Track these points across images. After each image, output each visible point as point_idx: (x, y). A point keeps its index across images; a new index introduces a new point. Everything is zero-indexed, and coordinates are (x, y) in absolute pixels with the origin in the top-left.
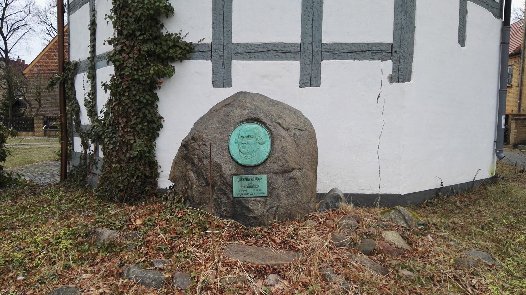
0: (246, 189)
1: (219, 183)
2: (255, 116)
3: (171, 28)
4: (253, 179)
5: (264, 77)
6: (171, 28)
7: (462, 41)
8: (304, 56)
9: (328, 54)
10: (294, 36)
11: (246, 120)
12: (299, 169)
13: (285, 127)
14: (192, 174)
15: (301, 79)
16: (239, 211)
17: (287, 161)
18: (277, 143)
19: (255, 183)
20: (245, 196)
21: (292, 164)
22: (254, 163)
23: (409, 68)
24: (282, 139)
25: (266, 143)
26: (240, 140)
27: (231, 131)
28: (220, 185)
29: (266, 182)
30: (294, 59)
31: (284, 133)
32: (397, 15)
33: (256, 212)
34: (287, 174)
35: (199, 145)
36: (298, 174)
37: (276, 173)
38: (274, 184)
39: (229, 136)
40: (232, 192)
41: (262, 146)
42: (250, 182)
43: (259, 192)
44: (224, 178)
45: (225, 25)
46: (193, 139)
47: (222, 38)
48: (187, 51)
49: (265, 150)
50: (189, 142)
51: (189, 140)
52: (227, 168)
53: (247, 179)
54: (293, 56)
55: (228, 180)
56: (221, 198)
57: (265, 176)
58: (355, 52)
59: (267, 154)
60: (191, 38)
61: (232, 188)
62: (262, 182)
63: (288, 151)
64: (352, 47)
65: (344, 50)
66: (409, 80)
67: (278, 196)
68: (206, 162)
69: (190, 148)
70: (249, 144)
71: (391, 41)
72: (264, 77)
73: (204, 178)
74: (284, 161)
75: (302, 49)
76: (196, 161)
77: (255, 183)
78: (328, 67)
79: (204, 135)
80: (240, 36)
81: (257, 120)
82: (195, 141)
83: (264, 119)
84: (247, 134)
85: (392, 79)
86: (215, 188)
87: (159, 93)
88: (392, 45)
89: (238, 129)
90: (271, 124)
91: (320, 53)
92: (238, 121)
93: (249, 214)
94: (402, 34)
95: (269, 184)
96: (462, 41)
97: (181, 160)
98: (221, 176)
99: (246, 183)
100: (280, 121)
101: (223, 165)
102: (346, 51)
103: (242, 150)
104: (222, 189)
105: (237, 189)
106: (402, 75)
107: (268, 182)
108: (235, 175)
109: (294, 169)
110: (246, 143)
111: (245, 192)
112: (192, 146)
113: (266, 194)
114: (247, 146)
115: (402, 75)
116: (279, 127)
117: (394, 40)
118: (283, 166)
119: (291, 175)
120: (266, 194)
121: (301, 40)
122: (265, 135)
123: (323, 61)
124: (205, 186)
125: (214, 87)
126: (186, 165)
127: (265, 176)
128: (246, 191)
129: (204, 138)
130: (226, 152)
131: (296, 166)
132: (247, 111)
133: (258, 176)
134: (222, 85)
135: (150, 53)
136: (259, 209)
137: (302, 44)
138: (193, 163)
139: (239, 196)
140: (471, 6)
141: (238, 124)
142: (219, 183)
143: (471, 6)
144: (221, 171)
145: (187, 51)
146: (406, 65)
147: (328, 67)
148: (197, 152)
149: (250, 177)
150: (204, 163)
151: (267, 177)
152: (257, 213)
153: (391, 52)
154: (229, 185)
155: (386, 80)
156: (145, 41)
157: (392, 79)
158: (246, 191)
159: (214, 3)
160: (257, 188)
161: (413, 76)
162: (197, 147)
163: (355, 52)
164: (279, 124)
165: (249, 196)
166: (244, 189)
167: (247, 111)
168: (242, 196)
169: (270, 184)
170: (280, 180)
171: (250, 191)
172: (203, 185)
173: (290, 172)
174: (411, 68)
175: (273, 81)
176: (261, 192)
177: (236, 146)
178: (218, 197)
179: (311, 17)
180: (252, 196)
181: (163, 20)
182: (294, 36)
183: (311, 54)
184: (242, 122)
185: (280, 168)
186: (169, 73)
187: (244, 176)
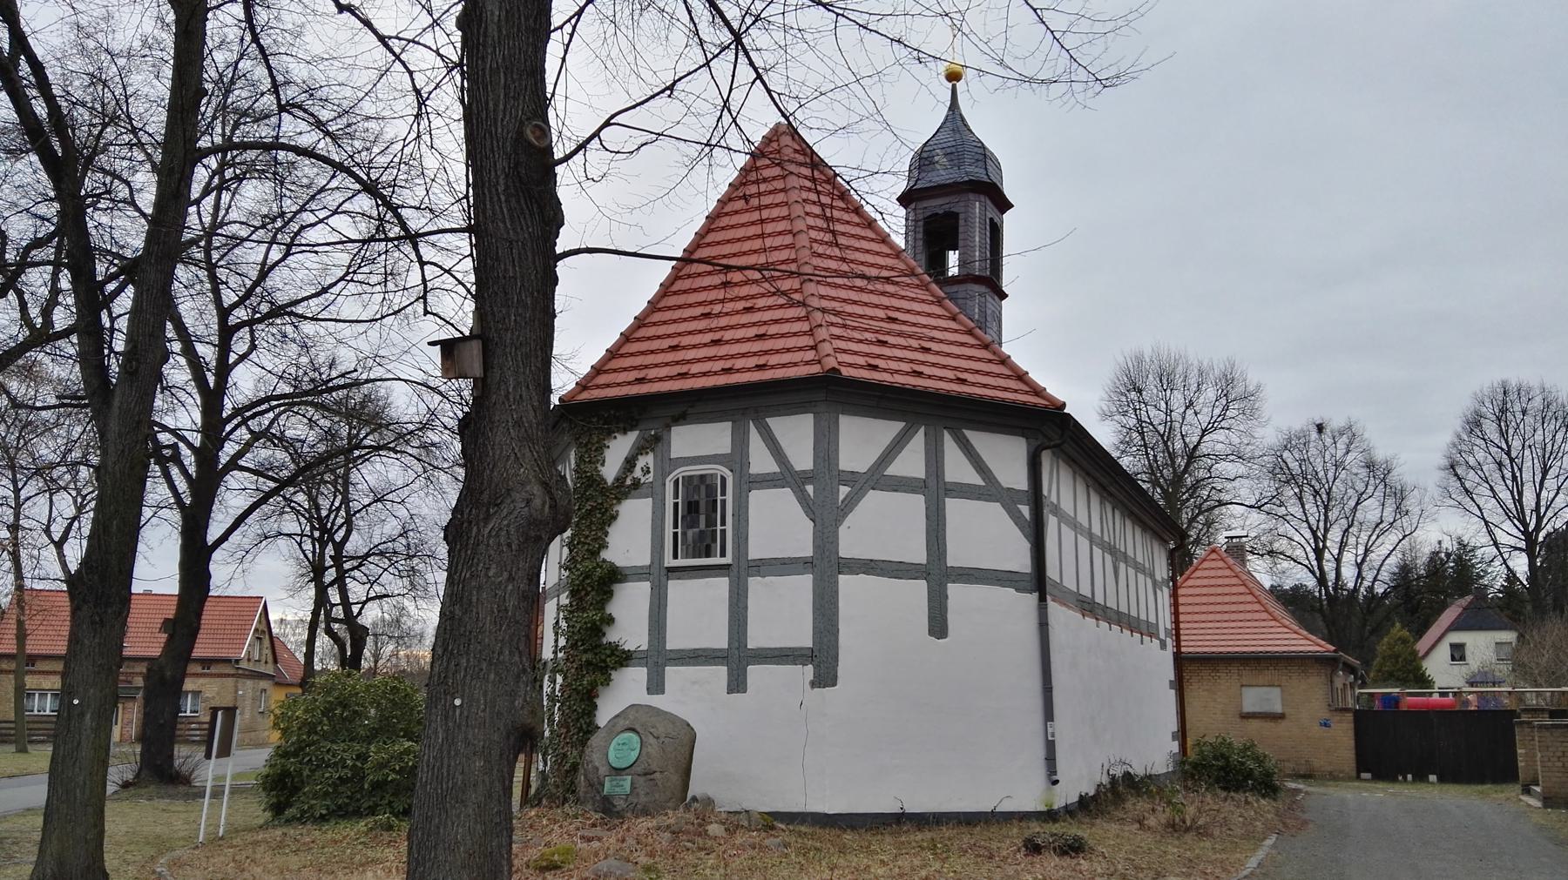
3: (612, 636)
5: (694, 683)
6: (612, 636)
10: (722, 642)
16: (607, 808)
21: (654, 767)
48: (624, 658)
52: (603, 770)
60: (629, 646)
66: (834, 684)
72: (694, 683)
78: (755, 672)
80: (673, 642)
81: (633, 730)
85: (813, 684)
87: (598, 701)
106: (826, 677)
115: (826, 677)
135: (589, 663)
136: (620, 804)
140: (559, 250)
143: (559, 250)
145: (624, 658)
147: (755, 672)
155: (808, 686)
156: (585, 651)
157: (813, 684)
161: (839, 681)
181: (606, 629)
182: (722, 642)
186: (607, 681)
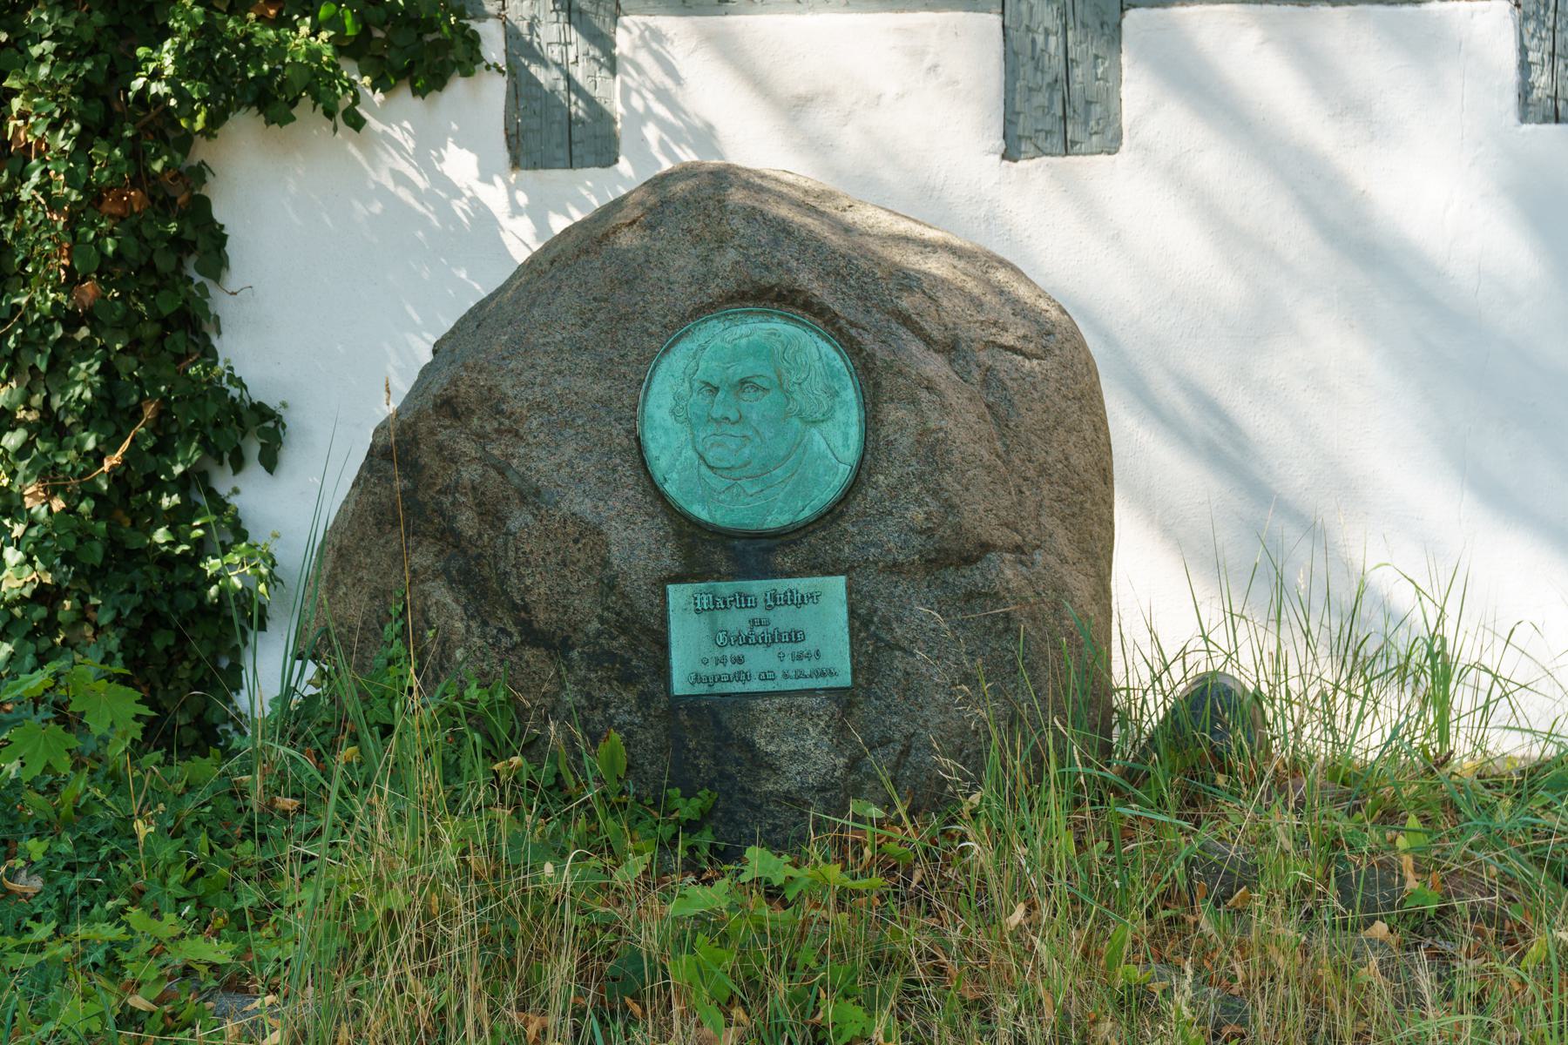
1: (595, 625)
4: (775, 600)
12: (1018, 549)
13: (936, 335)
14: (440, 593)
17: (950, 507)
18: (894, 413)
19: (783, 619)
20: (737, 687)
22: (777, 519)
24: (924, 395)
25: (840, 415)
26: (700, 400)
27: (648, 361)
28: (599, 634)
29: (842, 613)
31: (935, 366)
33: (795, 768)
34: (950, 575)
36: (1009, 573)
38: (886, 622)
39: (641, 383)
41: (814, 431)
42: (757, 613)
43: (806, 666)
44: (624, 595)
46: (449, 407)
49: (837, 442)
50: (423, 427)
51: (419, 416)
53: (744, 600)
55: (642, 605)
56: (607, 705)
57: (836, 586)
61: (664, 646)
62: (824, 612)
63: (956, 457)
68: (519, 519)
69: (425, 460)
70: (745, 422)
74: (934, 506)
76: (467, 522)
77: (783, 619)
79: (506, 386)
81: (783, 299)
82: (456, 415)
83: (818, 290)
86: (575, 654)
87: (219, 214)
89: (685, 347)
90: (861, 318)
92: (689, 306)
95: (859, 621)
97: (372, 531)
98: (610, 585)
99: (737, 620)
100: (906, 303)
101: (616, 533)
103: (709, 456)
104: (612, 656)
105: (690, 657)
107: (852, 613)
108: (678, 579)
109: (986, 547)
110: (733, 415)
111: (731, 669)
112: (441, 448)
113: (845, 679)
114: (735, 430)
116: (903, 332)
118: (928, 532)
119: (973, 576)
120: (845, 679)
122: (832, 374)
124: (514, 647)
125: (516, 164)
127: (836, 586)
129: (504, 399)
130: (626, 471)
131: (1000, 536)
132: (732, 255)
133: (802, 584)
134: (562, 153)
138: (449, 536)
139: (701, 689)
141: (684, 319)
142: (595, 625)
144: (606, 563)
148: (470, 473)
149: (757, 587)
150: (513, 525)
154: (646, 630)
158: (739, 660)
160: (799, 647)
162: (468, 447)
164: (905, 320)
165: (755, 686)
166: (729, 652)
169: (866, 623)
171: (759, 659)
172: (505, 642)
173: (968, 560)
177: (680, 434)
178: (589, 696)
180: (770, 686)
184: (703, 311)
185: (917, 541)
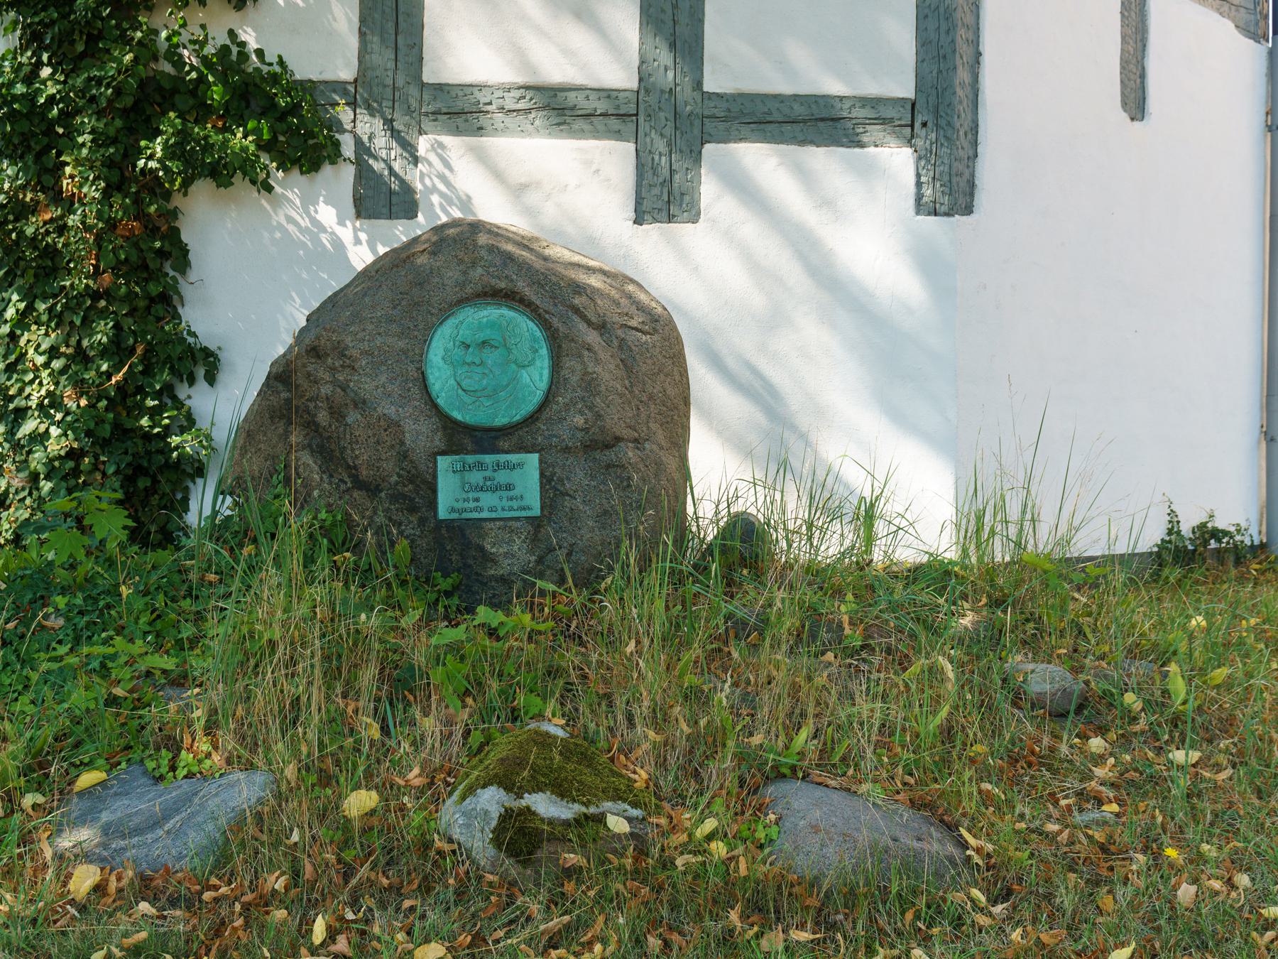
0: (476, 495)
2: (503, 285)
4: (498, 466)
7: (1135, 102)
8: (648, 129)
9: (722, 126)
11: (478, 296)
12: (636, 441)
13: (594, 319)
15: (639, 201)
18: (568, 363)
19: (502, 477)
20: (475, 515)
22: (501, 421)
23: (967, 173)
24: (586, 353)
25: (538, 363)
26: (459, 352)
27: (430, 329)
28: (397, 483)
29: (536, 475)
30: (618, 135)
31: (592, 337)
32: (926, 17)
35: (333, 369)
36: (631, 454)
37: (567, 450)
40: (433, 505)
42: (488, 473)
43: (515, 504)
45: (402, 25)
46: (315, 352)
47: (391, 65)
49: (535, 378)
53: (480, 466)
54: (616, 127)
55: (422, 467)
58: (804, 121)
59: (538, 396)
64: (796, 106)
65: (770, 113)
67: (573, 517)
68: (353, 417)
71: (910, 94)
73: (349, 467)
75: (642, 107)
76: (323, 417)
77: (502, 477)
81: (509, 297)
82: (319, 357)
83: (528, 292)
84: (481, 336)
88: (913, 105)
89: (451, 322)
91: (697, 123)
93: (485, 568)
94: (940, 72)
95: (546, 479)
96: (1135, 102)
99: (476, 477)
101: (408, 425)
102: (777, 116)
104: (404, 496)
105: (450, 496)
107: (542, 474)
108: (443, 453)
109: (618, 439)
111: (472, 505)
112: (309, 375)
113: (537, 512)
116: (576, 318)
117: (918, 89)
118: (586, 430)
119: (611, 455)
120: (537, 512)
121: (641, 80)
123: (707, 146)
126: (287, 434)
127: (534, 458)
128: (477, 500)
129: (346, 348)
130: (416, 391)
133: (514, 458)
134: (385, 211)
137: (642, 92)
138: (311, 425)
139: (455, 516)
144: (402, 443)
146: (955, 164)
148: (326, 390)
149: (489, 459)
150: (349, 420)
151: (541, 461)
152: (504, 567)
153: (912, 126)
154: (425, 482)
158: (477, 500)
159: (1125, 7)
160: (511, 493)
163: (804, 121)
164: (577, 311)
165: (485, 515)
166: (471, 495)
167: (480, 270)
168: (465, 515)
170: (578, 475)
171: (488, 499)
172: (343, 487)
173: (608, 446)
174: (973, 175)
175: (556, 193)
176: (523, 503)
177: (447, 371)
179: (669, 12)
180: (494, 515)
183: (673, 127)
187: (470, 459)
